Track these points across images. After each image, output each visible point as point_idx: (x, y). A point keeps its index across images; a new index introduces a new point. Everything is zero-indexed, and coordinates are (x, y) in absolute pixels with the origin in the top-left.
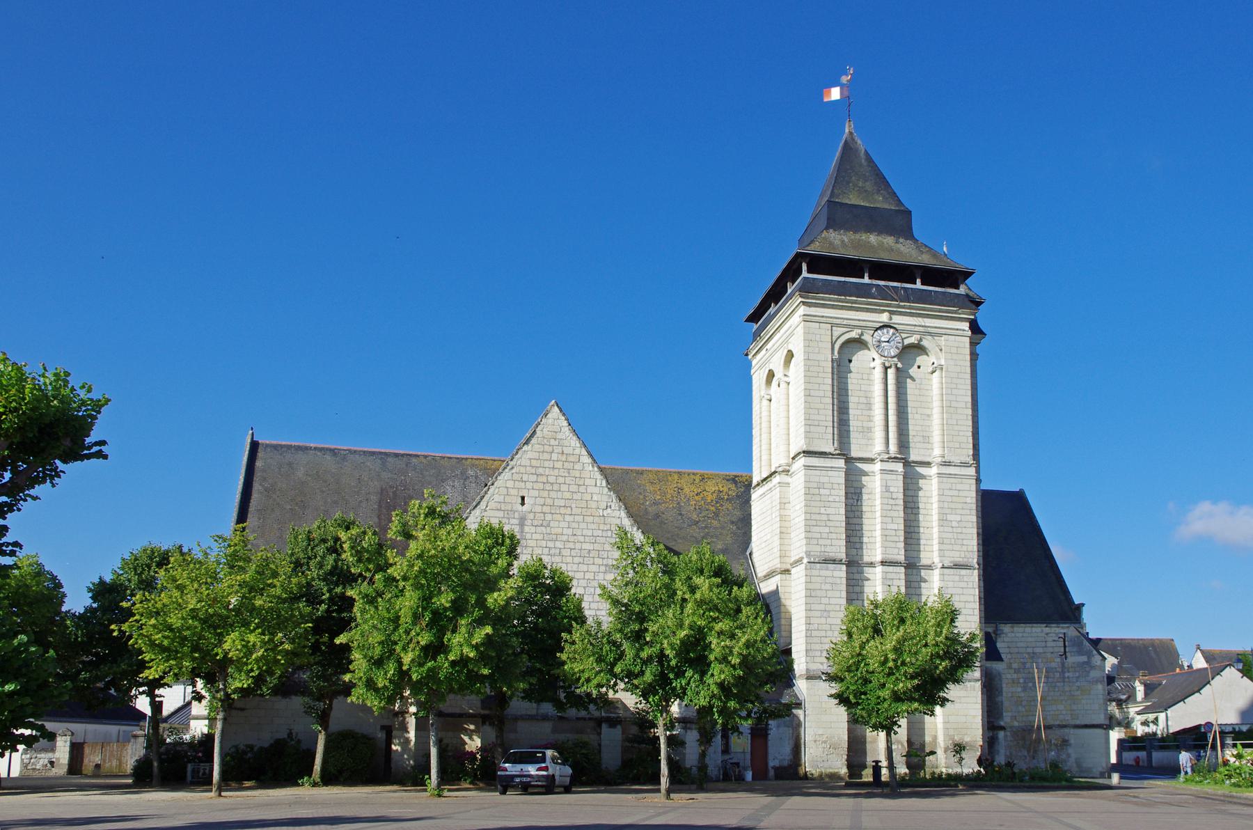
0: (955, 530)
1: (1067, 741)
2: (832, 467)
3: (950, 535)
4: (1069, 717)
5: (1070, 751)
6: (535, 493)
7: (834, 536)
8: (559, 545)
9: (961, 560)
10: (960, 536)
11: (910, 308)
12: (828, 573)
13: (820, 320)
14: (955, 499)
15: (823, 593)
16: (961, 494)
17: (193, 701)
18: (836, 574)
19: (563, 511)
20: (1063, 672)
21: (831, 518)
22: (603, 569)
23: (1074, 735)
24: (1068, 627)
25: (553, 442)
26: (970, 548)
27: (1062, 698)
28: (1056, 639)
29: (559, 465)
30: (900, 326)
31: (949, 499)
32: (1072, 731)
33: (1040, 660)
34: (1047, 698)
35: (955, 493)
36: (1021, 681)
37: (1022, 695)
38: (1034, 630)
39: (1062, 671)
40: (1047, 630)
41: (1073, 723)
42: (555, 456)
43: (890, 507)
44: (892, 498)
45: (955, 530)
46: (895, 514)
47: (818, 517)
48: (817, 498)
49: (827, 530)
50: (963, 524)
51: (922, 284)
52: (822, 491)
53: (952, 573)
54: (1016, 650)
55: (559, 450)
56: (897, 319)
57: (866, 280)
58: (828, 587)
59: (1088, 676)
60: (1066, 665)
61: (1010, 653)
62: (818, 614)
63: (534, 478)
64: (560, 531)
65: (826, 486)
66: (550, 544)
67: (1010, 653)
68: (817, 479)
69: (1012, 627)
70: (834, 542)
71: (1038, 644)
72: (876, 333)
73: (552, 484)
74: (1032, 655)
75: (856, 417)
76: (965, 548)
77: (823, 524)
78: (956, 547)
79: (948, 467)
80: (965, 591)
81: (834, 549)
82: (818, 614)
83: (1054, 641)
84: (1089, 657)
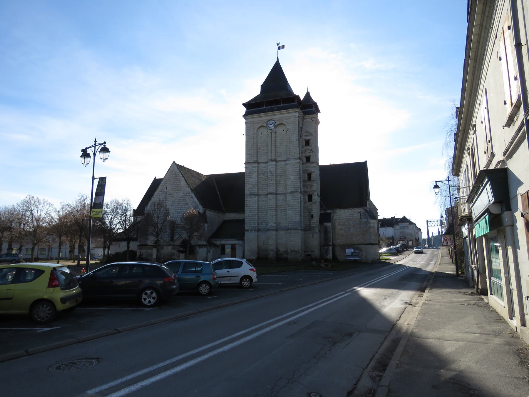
3: (290, 183)
6: (169, 186)
7: (253, 187)
8: (174, 199)
17: (156, 239)
18: (254, 199)
19: (175, 190)
21: (253, 182)
22: (184, 204)
25: (173, 172)
29: (174, 178)
33: (351, 221)
38: (348, 210)
40: (353, 210)
42: (174, 176)
43: (271, 176)
46: (273, 178)
47: (249, 182)
49: (251, 186)
51: (282, 104)
52: (250, 174)
55: (174, 174)
57: (265, 107)
58: (252, 203)
61: (339, 219)
63: (169, 182)
64: (174, 195)
66: (172, 199)
67: (339, 219)
69: (340, 210)
73: (173, 183)
76: (295, 186)
83: (357, 214)
84: (368, 220)
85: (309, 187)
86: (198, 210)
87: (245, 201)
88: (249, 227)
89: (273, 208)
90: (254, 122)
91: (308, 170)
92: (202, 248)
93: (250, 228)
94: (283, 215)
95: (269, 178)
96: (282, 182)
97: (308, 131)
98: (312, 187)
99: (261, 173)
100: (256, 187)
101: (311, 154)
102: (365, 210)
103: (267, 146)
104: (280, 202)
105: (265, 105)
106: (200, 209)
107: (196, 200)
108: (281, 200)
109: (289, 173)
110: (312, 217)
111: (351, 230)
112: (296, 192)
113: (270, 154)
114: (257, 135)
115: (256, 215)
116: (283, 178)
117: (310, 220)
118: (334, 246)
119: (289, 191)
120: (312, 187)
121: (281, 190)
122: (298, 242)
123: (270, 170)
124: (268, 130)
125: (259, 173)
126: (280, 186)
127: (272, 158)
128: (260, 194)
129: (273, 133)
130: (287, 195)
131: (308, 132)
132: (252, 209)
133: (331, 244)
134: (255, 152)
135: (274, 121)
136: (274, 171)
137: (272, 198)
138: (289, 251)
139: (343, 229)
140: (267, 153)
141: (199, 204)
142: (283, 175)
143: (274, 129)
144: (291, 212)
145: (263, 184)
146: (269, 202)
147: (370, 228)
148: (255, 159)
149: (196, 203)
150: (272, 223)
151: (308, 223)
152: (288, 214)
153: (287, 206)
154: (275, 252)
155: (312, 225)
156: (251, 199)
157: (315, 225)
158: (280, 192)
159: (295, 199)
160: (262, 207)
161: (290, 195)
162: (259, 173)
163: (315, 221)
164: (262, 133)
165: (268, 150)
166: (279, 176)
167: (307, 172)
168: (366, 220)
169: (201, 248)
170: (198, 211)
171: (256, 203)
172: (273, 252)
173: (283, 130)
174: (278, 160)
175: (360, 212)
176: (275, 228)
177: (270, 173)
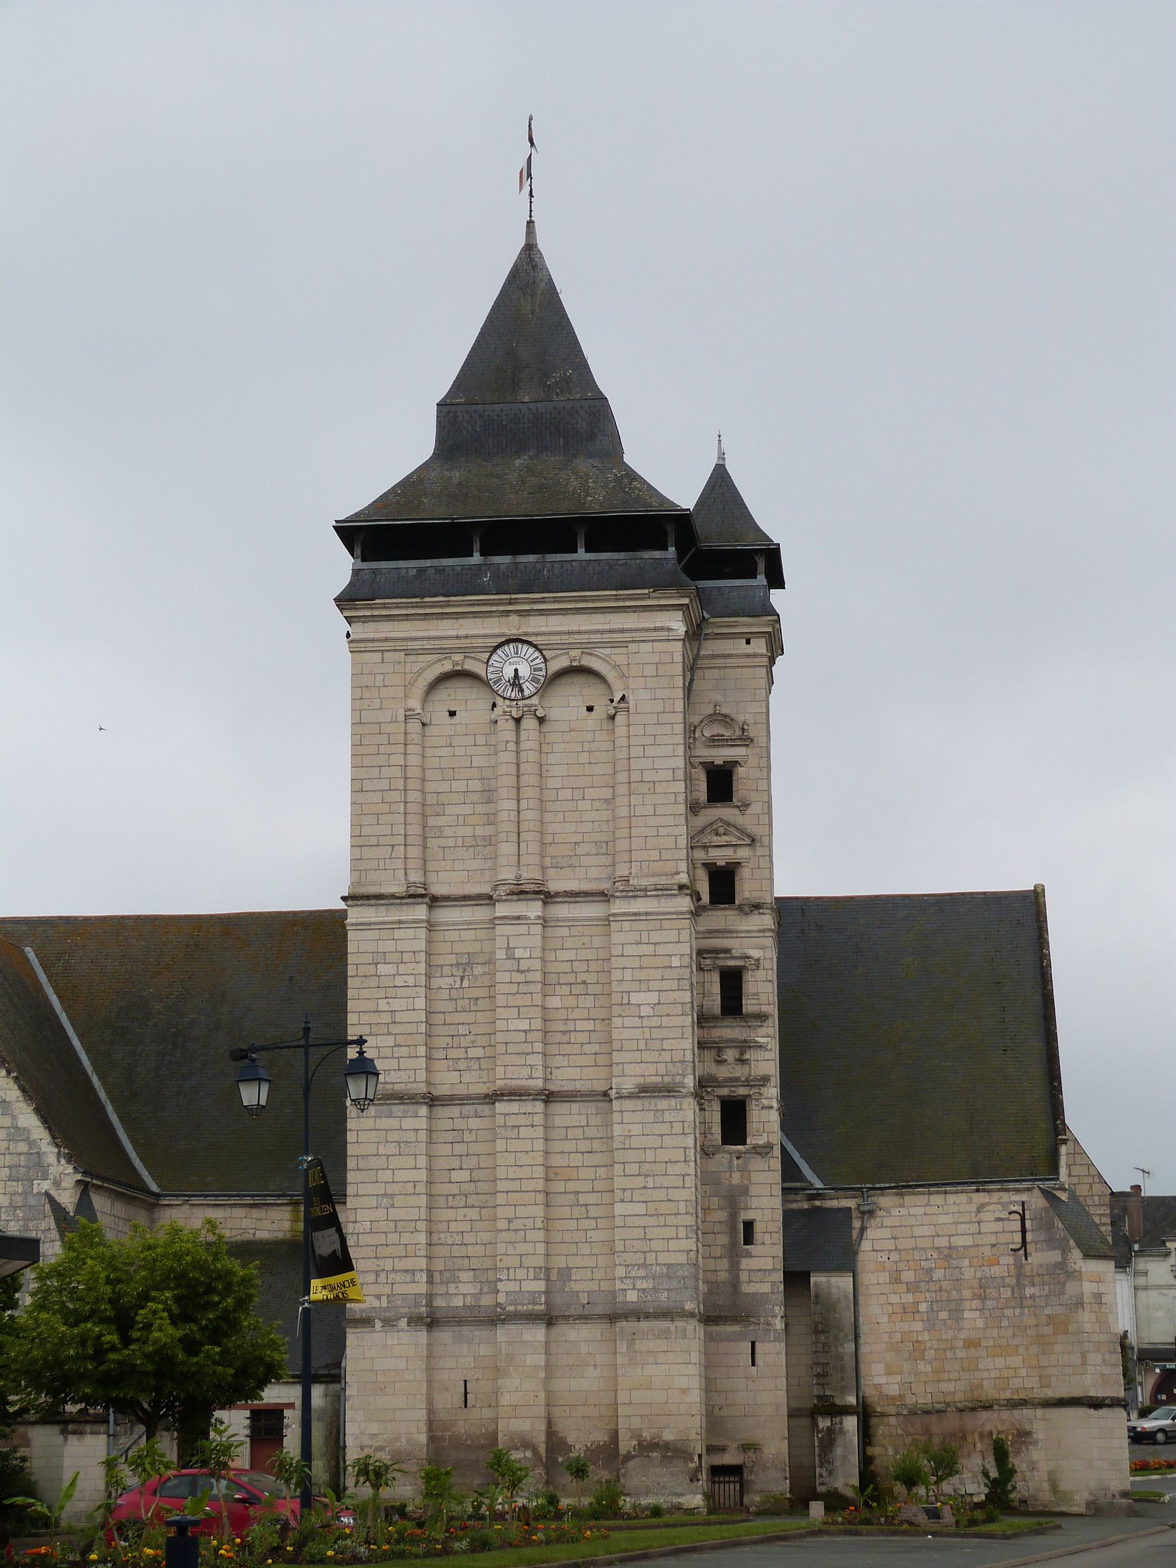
0: (646, 1022)
1: (1028, 1434)
2: (400, 922)
3: (637, 1034)
4: (1033, 1382)
5: (1036, 1454)
7: (404, 1051)
9: (659, 1079)
10: (656, 1033)
11: (555, 600)
12: (393, 1123)
13: (384, 646)
14: (646, 962)
15: (382, 1162)
16: (661, 950)
18: (408, 1123)
20: (1019, 1285)
21: (399, 1017)
23: (1039, 1422)
24: (1029, 1189)
26: (678, 1056)
27: (1018, 1341)
28: (1004, 1215)
30: (540, 638)
31: (636, 963)
32: (1040, 1412)
33: (966, 1262)
34: (983, 1343)
35: (649, 950)
36: (923, 1307)
37: (926, 1337)
39: (1018, 1283)
40: (981, 1198)
41: (1043, 1396)
43: (514, 988)
44: (518, 971)
45: (646, 1022)
46: (527, 1000)
47: (374, 1018)
48: (373, 982)
49: (390, 1041)
50: (661, 1010)
52: (383, 969)
53: (640, 1108)
54: (911, 1243)
56: (535, 625)
57: (476, 558)
58: (392, 1149)
59: (1063, 1294)
60: (1027, 1268)
62: (373, 1202)
65: (389, 958)
68: (371, 947)
70: (405, 1063)
71: (962, 1228)
72: (495, 657)
74: (946, 1252)
75: (461, 819)
76: (666, 1056)
77: (384, 1030)
78: (646, 1056)
79: (633, 900)
80: (667, 1141)
81: (403, 1076)
82: (373, 1202)
83: (999, 1219)
85: (730, 1055)
86: (46, 1186)
87: (351, 1137)
88: (378, 1297)
89: (527, 1185)
90: (411, 645)
91: (727, 951)
92: (81, 1433)
93: (384, 1304)
94: (584, 1224)
95: (501, 1000)
96: (580, 1025)
97: (725, 711)
98: (747, 1056)
99: (451, 959)
100: (422, 1050)
101: (743, 853)
102: (1048, 1195)
103: (489, 795)
104: (569, 1146)
105: (477, 546)
106: (57, 1184)
107: (28, 1119)
108: (571, 1133)
109: (628, 975)
110: (749, 1239)
111: (967, 1315)
112: (668, 1090)
113: (507, 849)
114: (424, 725)
115: (422, 1226)
116: (589, 1002)
117: (734, 1256)
118: (865, 1414)
119: (629, 1085)
120: (747, 1056)
121: (575, 1073)
122: (684, 1391)
123: (508, 948)
124: (499, 701)
125: (437, 960)
126: (566, 1049)
127: (518, 878)
128: (442, 1091)
129: (529, 723)
130: (616, 1105)
131: (726, 720)
132: (395, 1189)
133: (852, 1400)
134: (415, 830)
135: (535, 646)
136: (538, 953)
137: (522, 1120)
138: (626, 1445)
139: (923, 1307)
140: (490, 841)
141: (49, 1151)
142: (584, 982)
143: (535, 701)
144: (640, 1209)
145: (462, 1030)
146: (500, 1145)
147: (1080, 1304)
148: (415, 877)
149: (31, 1143)
150: (521, 1274)
151: (723, 1276)
152: (619, 1222)
153: (618, 1169)
154: (542, 1449)
155: (747, 1288)
156: (384, 1123)
157: (765, 1288)
158: (568, 1087)
159: (665, 1129)
160: (457, 1176)
161: (628, 1104)
162: (437, 960)
163: (768, 1264)
164: (452, 714)
165: (491, 819)
166: (565, 990)
167: (721, 963)
168: (1055, 1256)
169: (74, 1433)
170: (47, 1194)
171: (422, 1148)
172: (529, 1454)
173: (590, 709)
174: (553, 886)
175: (1019, 1208)
176: (543, 1307)
177: (511, 964)
